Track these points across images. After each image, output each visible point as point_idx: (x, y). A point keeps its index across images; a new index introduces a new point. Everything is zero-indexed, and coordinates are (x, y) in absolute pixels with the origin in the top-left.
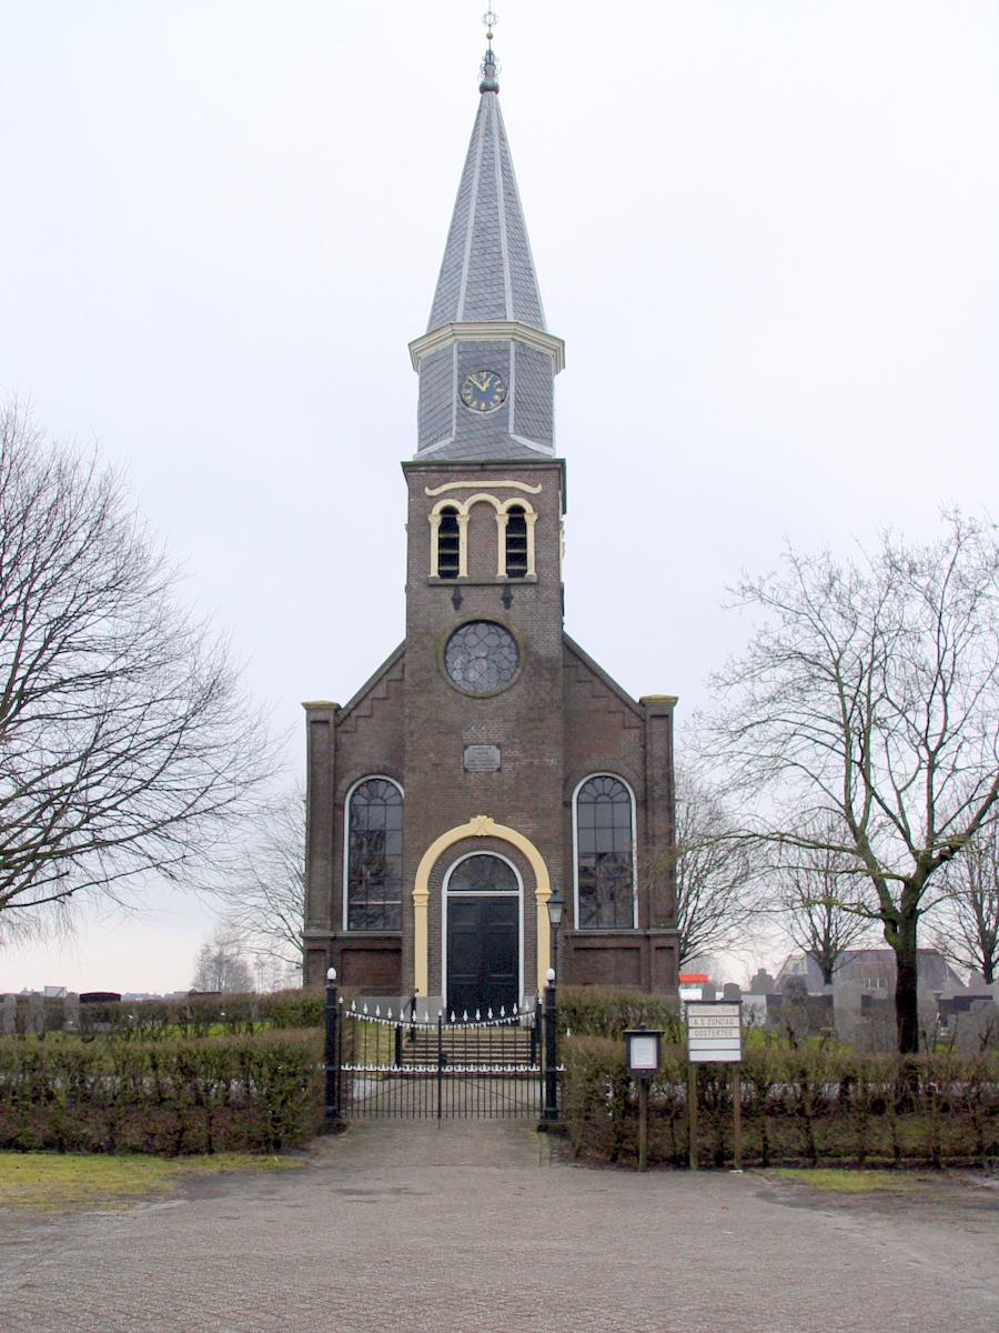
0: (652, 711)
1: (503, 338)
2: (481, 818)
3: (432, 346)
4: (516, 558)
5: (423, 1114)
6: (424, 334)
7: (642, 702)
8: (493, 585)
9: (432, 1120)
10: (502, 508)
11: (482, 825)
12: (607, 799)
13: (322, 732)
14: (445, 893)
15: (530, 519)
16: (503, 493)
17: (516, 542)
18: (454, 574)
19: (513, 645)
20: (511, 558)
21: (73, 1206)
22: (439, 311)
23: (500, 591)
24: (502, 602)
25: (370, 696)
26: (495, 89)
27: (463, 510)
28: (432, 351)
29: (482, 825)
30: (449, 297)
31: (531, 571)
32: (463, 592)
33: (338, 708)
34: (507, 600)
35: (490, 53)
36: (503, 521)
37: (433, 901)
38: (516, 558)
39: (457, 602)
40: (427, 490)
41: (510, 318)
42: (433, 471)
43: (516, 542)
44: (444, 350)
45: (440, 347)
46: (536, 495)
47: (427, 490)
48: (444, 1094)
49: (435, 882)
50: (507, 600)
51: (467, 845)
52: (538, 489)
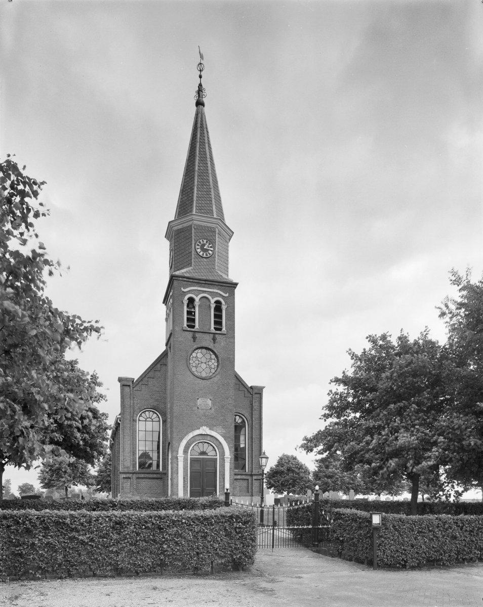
0: (256, 391)
1: (214, 226)
2: (204, 428)
3: (181, 224)
4: (218, 323)
5: (266, 546)
6: (173, 219)
7: (251, 387)
8: (209, 333)
9: (270, 549)
10: (213, 301)
11: (204, 430)
12: (151, 420)
13: (127, 389)
14: (189, 457)
15: (224, 307)
16: (214, 294)
17: (218, 316)
18: (193, 327)
19: (216, 359)
20: (216, 323)
21: (189, 587)
22: (182, 208)
23: (212, 335)
24: (212, 340)
25: (147, 376)
26: (203, 105)
27: (197, 299)
28: (180, 227)
29: (204, 430)
30: (187, 203)
31: (224, 329)
32: (197, 335)
33: (132, 380)
34: (214, 340)
35: (200, 85)
36: (213, 306)
37: (185, 459)
38: (218, 323)
39: (194, 338)
40: (182, 288)
41: (215, 216)
42: (184, 281)
43: (218, 316)
44: (187, 227)
45: (185, 225)
46: (226, 297)
47: (182, 288)
48: (272, 538)
49: (185, 452)
50: (214, 340)
51: (198, 438)
52: (227, 295)
